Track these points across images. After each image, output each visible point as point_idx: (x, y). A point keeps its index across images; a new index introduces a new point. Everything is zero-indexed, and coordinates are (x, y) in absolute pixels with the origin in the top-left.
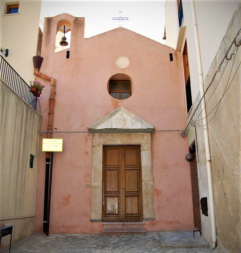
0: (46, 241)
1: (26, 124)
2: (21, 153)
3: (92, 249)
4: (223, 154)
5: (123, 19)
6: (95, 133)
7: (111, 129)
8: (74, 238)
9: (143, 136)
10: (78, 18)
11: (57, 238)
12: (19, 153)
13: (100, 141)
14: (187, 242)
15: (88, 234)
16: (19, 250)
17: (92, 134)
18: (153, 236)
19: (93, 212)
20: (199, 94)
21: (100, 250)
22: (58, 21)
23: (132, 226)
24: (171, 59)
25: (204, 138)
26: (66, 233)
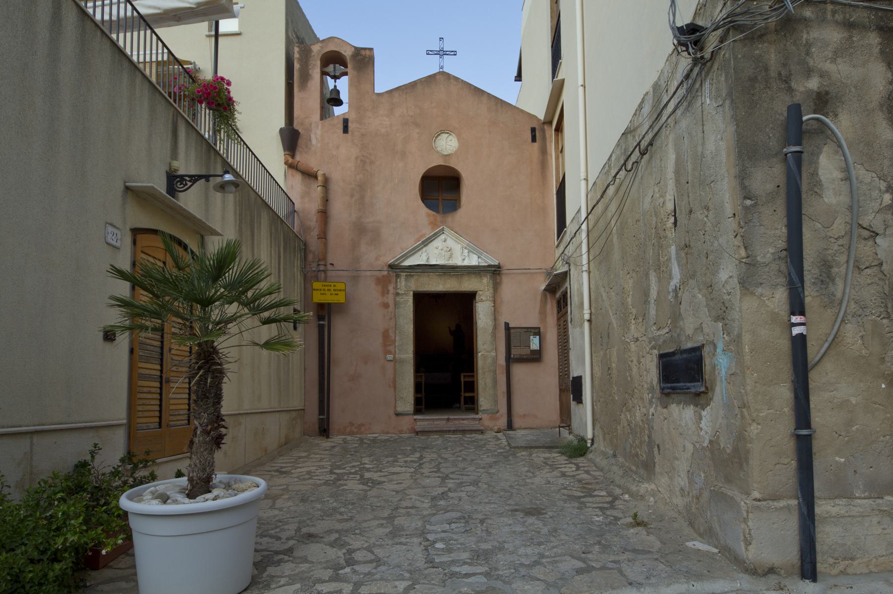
4: (610, 311)
5: (447, 53)
13: (407, 288)
15: (392, 434)
20: (578, 212)
22: (322, 54)
23: (462, 422)
24: (534, 139)
25: (582, 283)
26: (357, 433)
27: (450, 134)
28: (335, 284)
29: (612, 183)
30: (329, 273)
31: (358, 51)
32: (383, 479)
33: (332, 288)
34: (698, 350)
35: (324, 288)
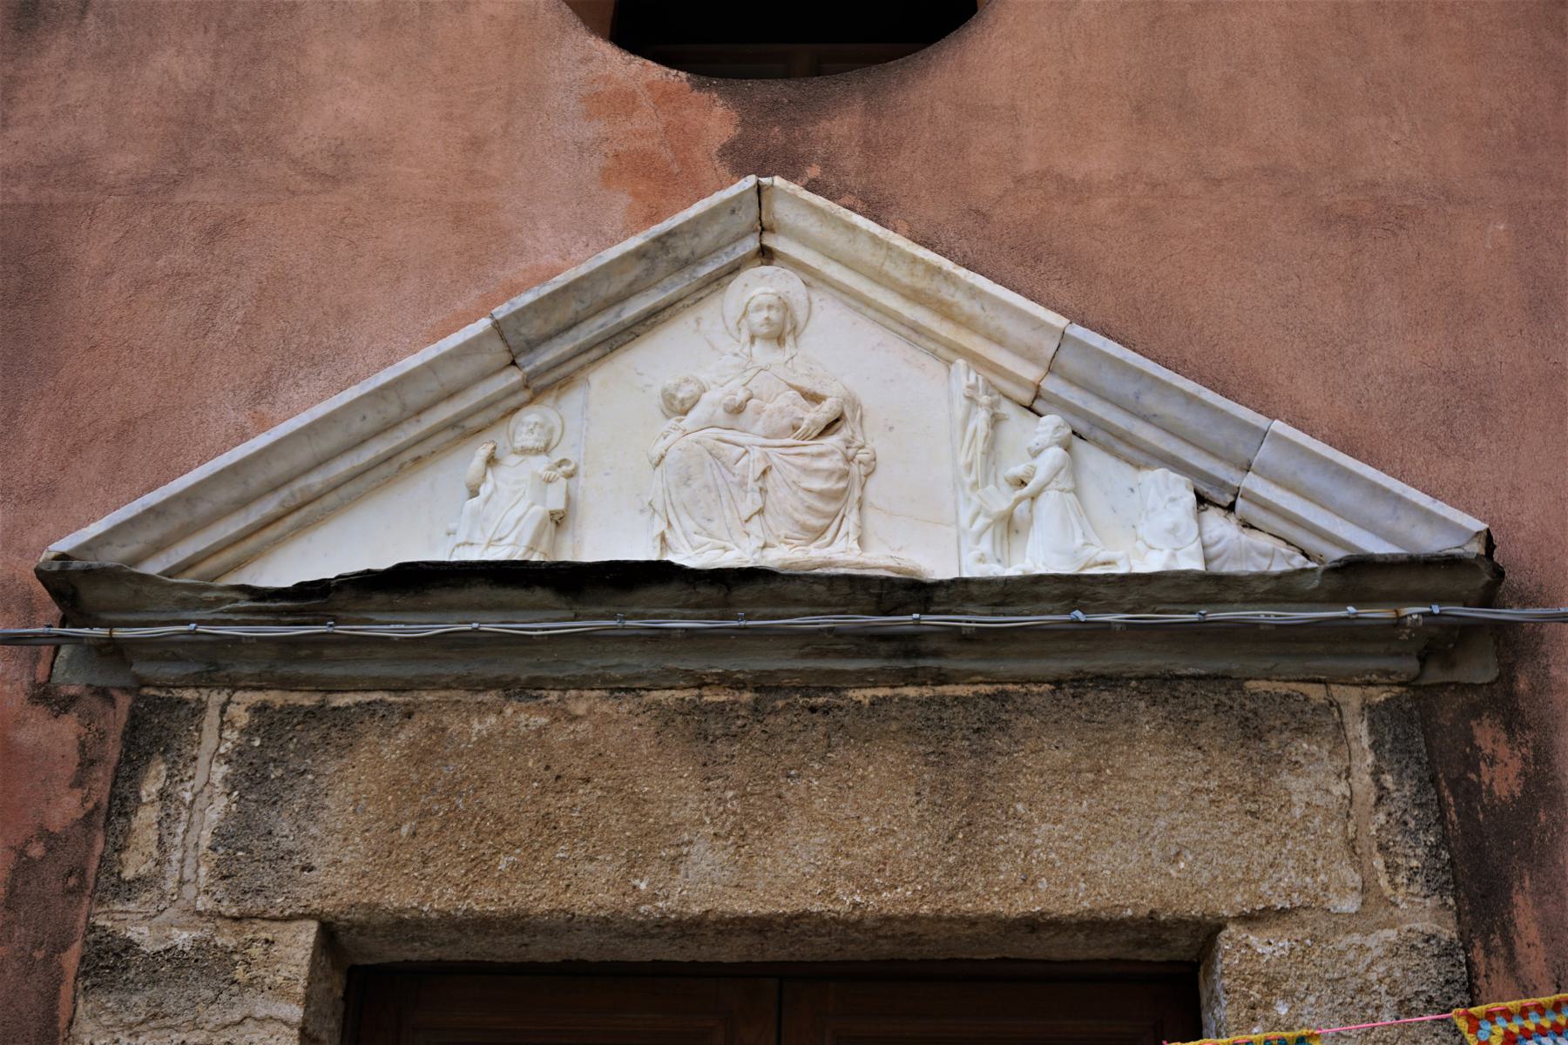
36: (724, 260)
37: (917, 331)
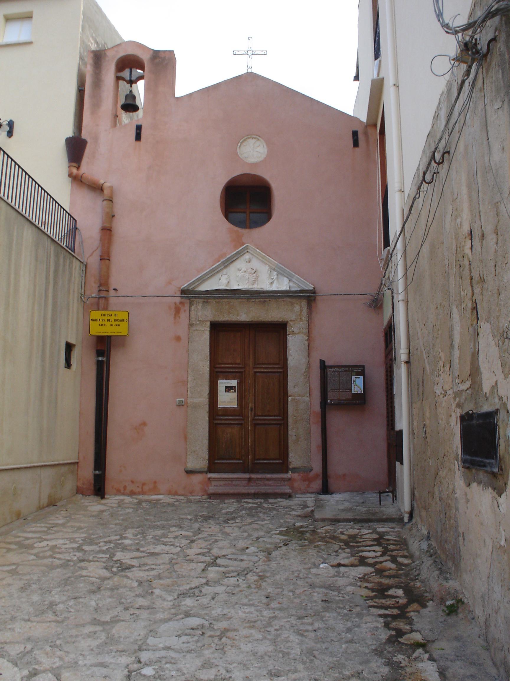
0: (99, 507)
1: (55, 283)
2: (48, 341)
3: (185, 522)
5: (256, 53)
6: (195, 298)
7: (227, 290)
8: (486, 632)
9: (292, 304)
10: (159, 51)
11: (120, 504)
12: (44, 342)
14: (364, 512)
16: (50, 522)
17: (189, 301)
18: (305, 502)
19: (190, 455)
21: (200, 523)
24: (356, 144)
26: (139, 493)
27: (258, 140)
28: (116, 313)
29: (417, 196)
30: (112, 301)
31: (156, 55)
32: (135, 562)
33: (113, 318)
34: (491, 416)
35: (103, 318)
36: (243, 253)
37: (262, 261)
